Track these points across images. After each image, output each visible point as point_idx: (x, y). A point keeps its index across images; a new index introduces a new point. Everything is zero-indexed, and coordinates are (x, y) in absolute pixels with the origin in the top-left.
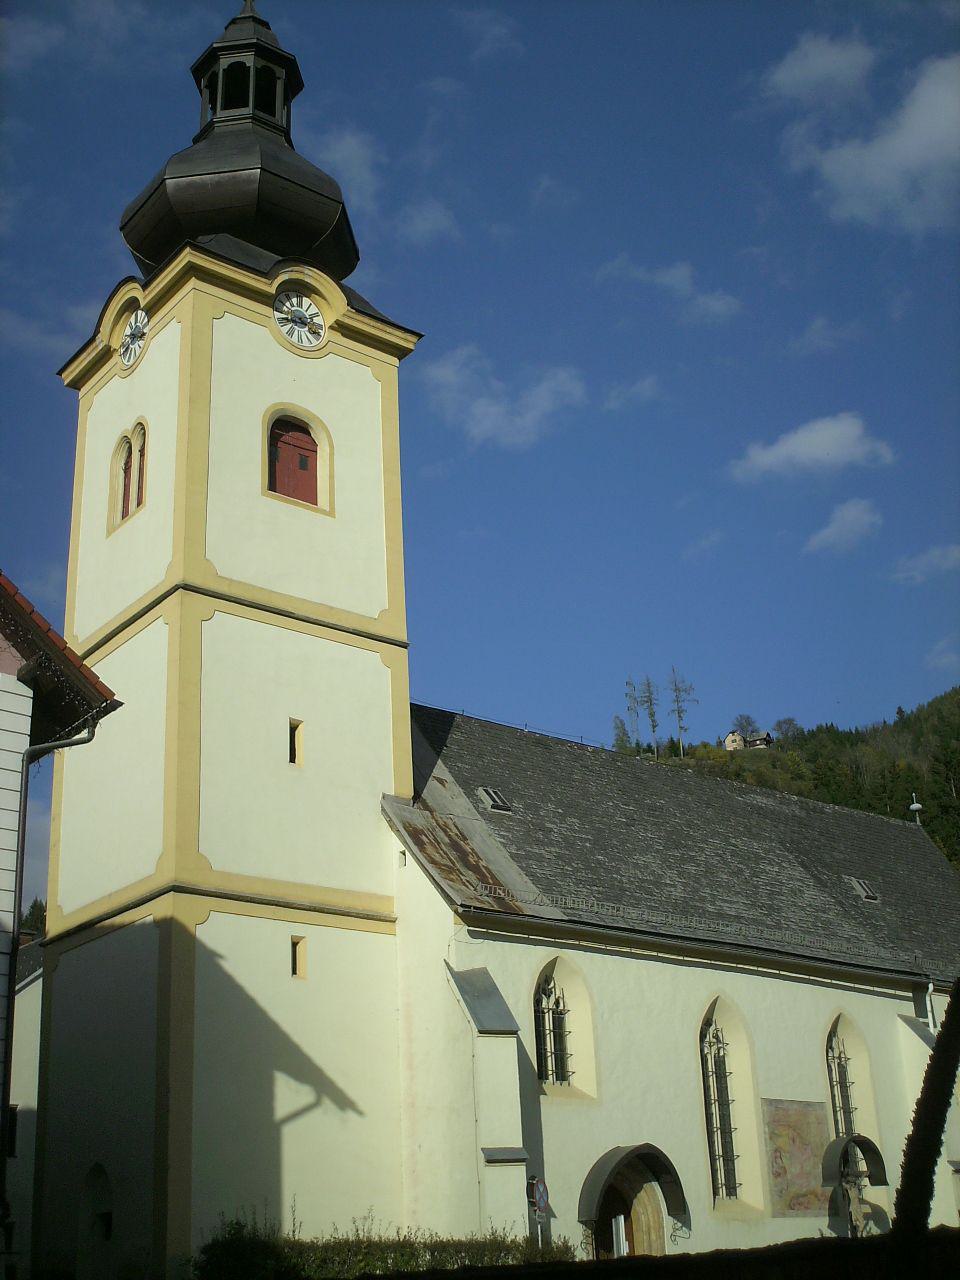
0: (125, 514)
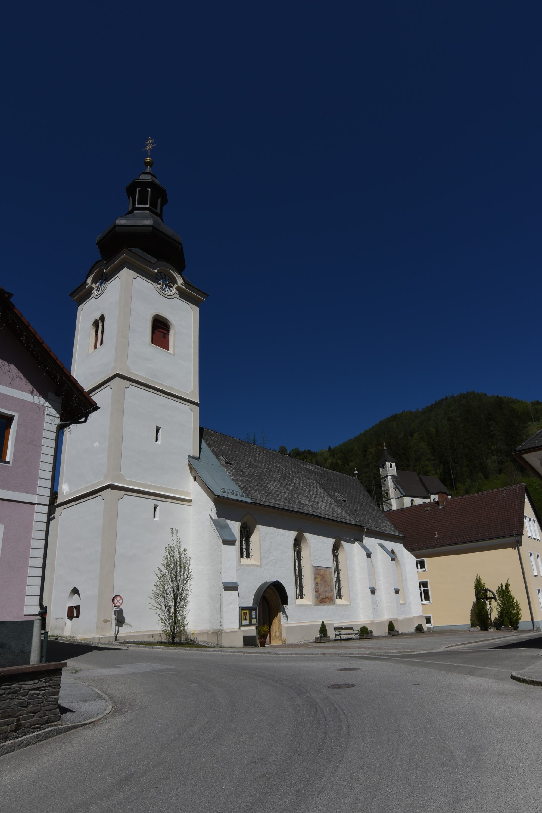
0: (95, 347)
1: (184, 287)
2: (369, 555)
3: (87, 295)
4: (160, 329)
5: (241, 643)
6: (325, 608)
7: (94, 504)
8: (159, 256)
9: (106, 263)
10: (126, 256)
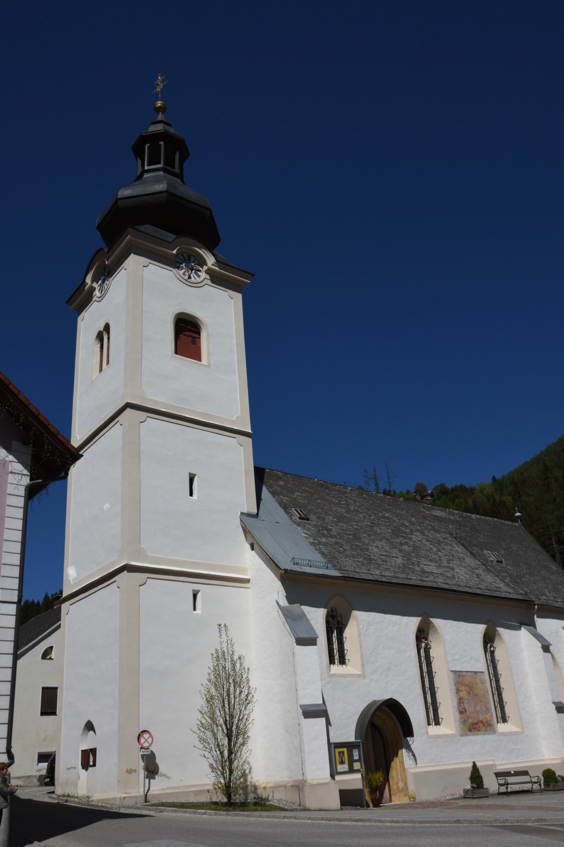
0: (101, 370)
1: (217, 269)
2: (546, 648)
3: (88, 299)
4: (187, 333)
5: (335, 802)
6: (478, 740)
7: (107, 595)
8: (179, 229)
9: (108, 252)
10: (133, 238)
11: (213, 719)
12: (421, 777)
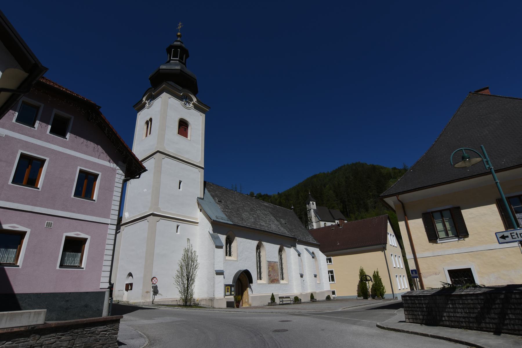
0: (146, 136)
2: (299, 255)
3: (143, 107)
4: (183, 126)
5: (225, 305)
8: (183, 85)
11: (182, 275)
12: (254, 298)
